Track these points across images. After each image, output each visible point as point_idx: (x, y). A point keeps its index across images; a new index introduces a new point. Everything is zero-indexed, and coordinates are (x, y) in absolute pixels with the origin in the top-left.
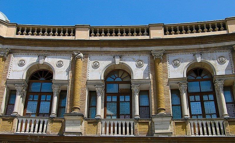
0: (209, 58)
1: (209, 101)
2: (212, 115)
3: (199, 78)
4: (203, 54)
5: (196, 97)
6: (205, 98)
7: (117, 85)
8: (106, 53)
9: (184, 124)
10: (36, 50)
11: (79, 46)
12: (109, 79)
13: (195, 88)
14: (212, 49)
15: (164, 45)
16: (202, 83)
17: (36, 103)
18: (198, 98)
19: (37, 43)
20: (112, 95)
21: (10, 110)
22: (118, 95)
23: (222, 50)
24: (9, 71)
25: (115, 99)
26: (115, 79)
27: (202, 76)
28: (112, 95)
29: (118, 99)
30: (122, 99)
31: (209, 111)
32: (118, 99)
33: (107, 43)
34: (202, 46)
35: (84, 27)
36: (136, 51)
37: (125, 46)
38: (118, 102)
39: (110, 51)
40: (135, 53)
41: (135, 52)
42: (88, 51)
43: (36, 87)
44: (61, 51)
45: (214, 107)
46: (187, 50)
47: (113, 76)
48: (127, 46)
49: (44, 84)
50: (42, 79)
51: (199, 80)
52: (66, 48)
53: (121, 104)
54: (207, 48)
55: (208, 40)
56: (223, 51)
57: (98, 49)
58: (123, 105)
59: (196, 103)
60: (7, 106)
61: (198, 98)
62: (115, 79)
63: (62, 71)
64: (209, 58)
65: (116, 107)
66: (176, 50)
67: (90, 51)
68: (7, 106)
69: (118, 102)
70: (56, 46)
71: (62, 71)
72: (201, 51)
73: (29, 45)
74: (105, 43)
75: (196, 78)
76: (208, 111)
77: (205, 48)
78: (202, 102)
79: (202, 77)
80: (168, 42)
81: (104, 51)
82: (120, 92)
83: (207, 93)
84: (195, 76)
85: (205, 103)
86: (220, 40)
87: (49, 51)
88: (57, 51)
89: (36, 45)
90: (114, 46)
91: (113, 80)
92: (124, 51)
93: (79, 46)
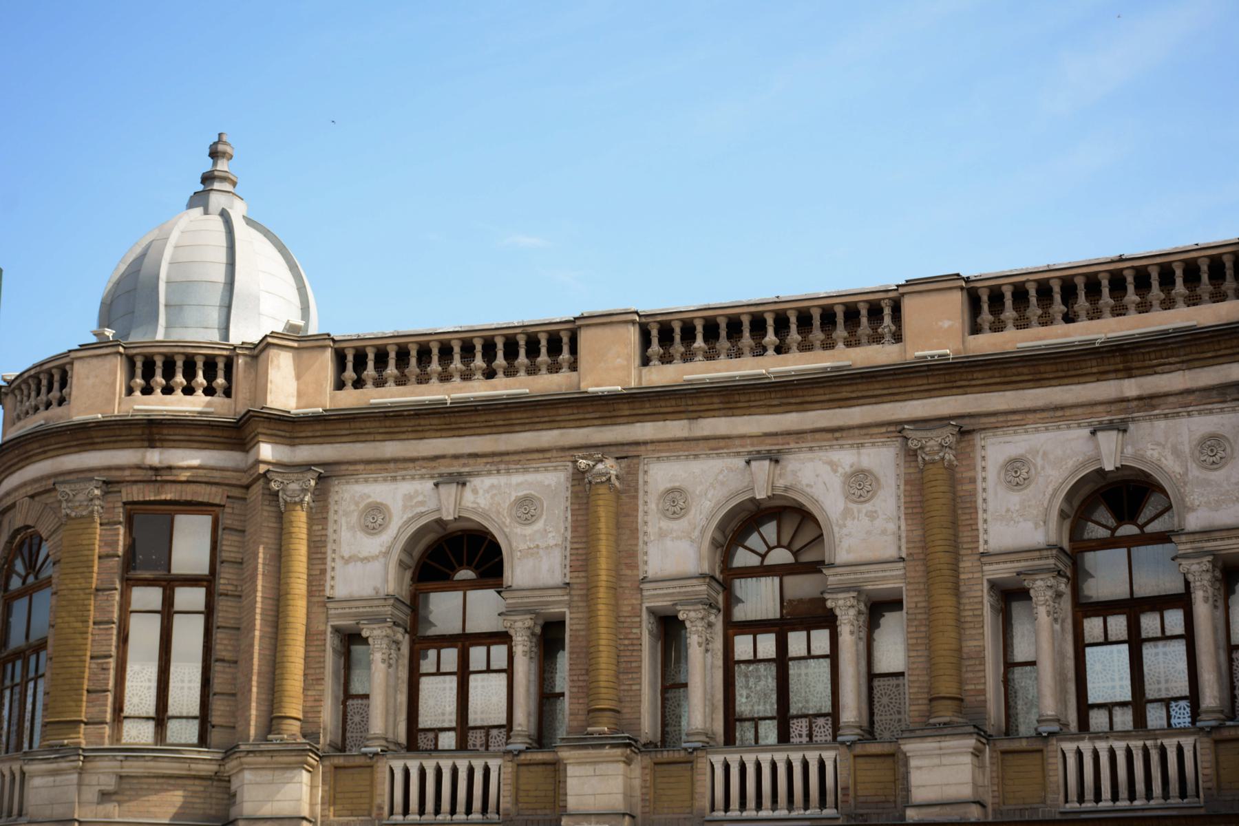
0: (1158, 444)
1: (1164, 637)
2: (1173, 704)
3: (1128, 530)
4: (1132, 427)
5: (1111, 620)
6: (1150, 624)
7: (777, 580)
8: (713, 443)
9: (1038, 755)
10: (425, 459)
11: (596, 422)
12: (743, 558)
13: (1108, 575)
14: (1171, 399)
15: (964, 389)
16: (1140, 552)
17: (452, 683)
18: (1118, 625)
19: (422, 422)
20: (755, 627)
21: (357, 719)
22: (780, 627)
23: (1216, 406)
24: (329, 564)
25: (767, 645)
26: (763, 556)
27: (1141, 520)
28: (755, 627)
29: (782, 645)
30: (796, 642)
31: (1163, 686)
32: (782, 645)
33: (716, 400)
34: (1131, 387)
35: (611, 323)
36: (840, 429)
37: (794, 407)
38: (782, 660)
39: (729, 438)
40: (837, 439)
41: (836, 433)
42: (637, 444)
43: (445, 609)
44: (523, 452)
45: (1183, 665)
46: (1062, 408)
47: (754, 540)
48: (803, 406)
49: (473, 595)
50: (465, 574)
51: (1129, 543)
52: (544, 433)
53: (794, 669)
54: (1152, 397)
55: (1153, 356)
56: (1222, 410)
57: (676, 428)
58: (803, 671)
59: (1112, 652)
60: (345, 706)
61: (1118, 625)
62: (767, 553)
63: (538, 546)
64: (1158, 444)
65: (771, 683)
66: (1014, 412)
67: (645, 443)
68: (345, 706)
69: (782, 660)
70: (503, 429)
71: (538, 546)
72: (1126, 410)
73: (391, 435)
74: (705, 400)
75: (1113, 530)
76: (1156, 686)
77: (1140, 398)
78: (1135, 643)
79: (1141, 527)
80: (980, 375)
81: (706, 439)
82: (788, 614)
83: (1160, 603)
84: (1111, 522)
85: (1148, 651)
86: (1209, 355)
87: (475, 456)
88: (507, 454)
89: (421, 435)
90: (748, 410)
91: (754, 561)
92: (789, 433)
93: (599, 422)
